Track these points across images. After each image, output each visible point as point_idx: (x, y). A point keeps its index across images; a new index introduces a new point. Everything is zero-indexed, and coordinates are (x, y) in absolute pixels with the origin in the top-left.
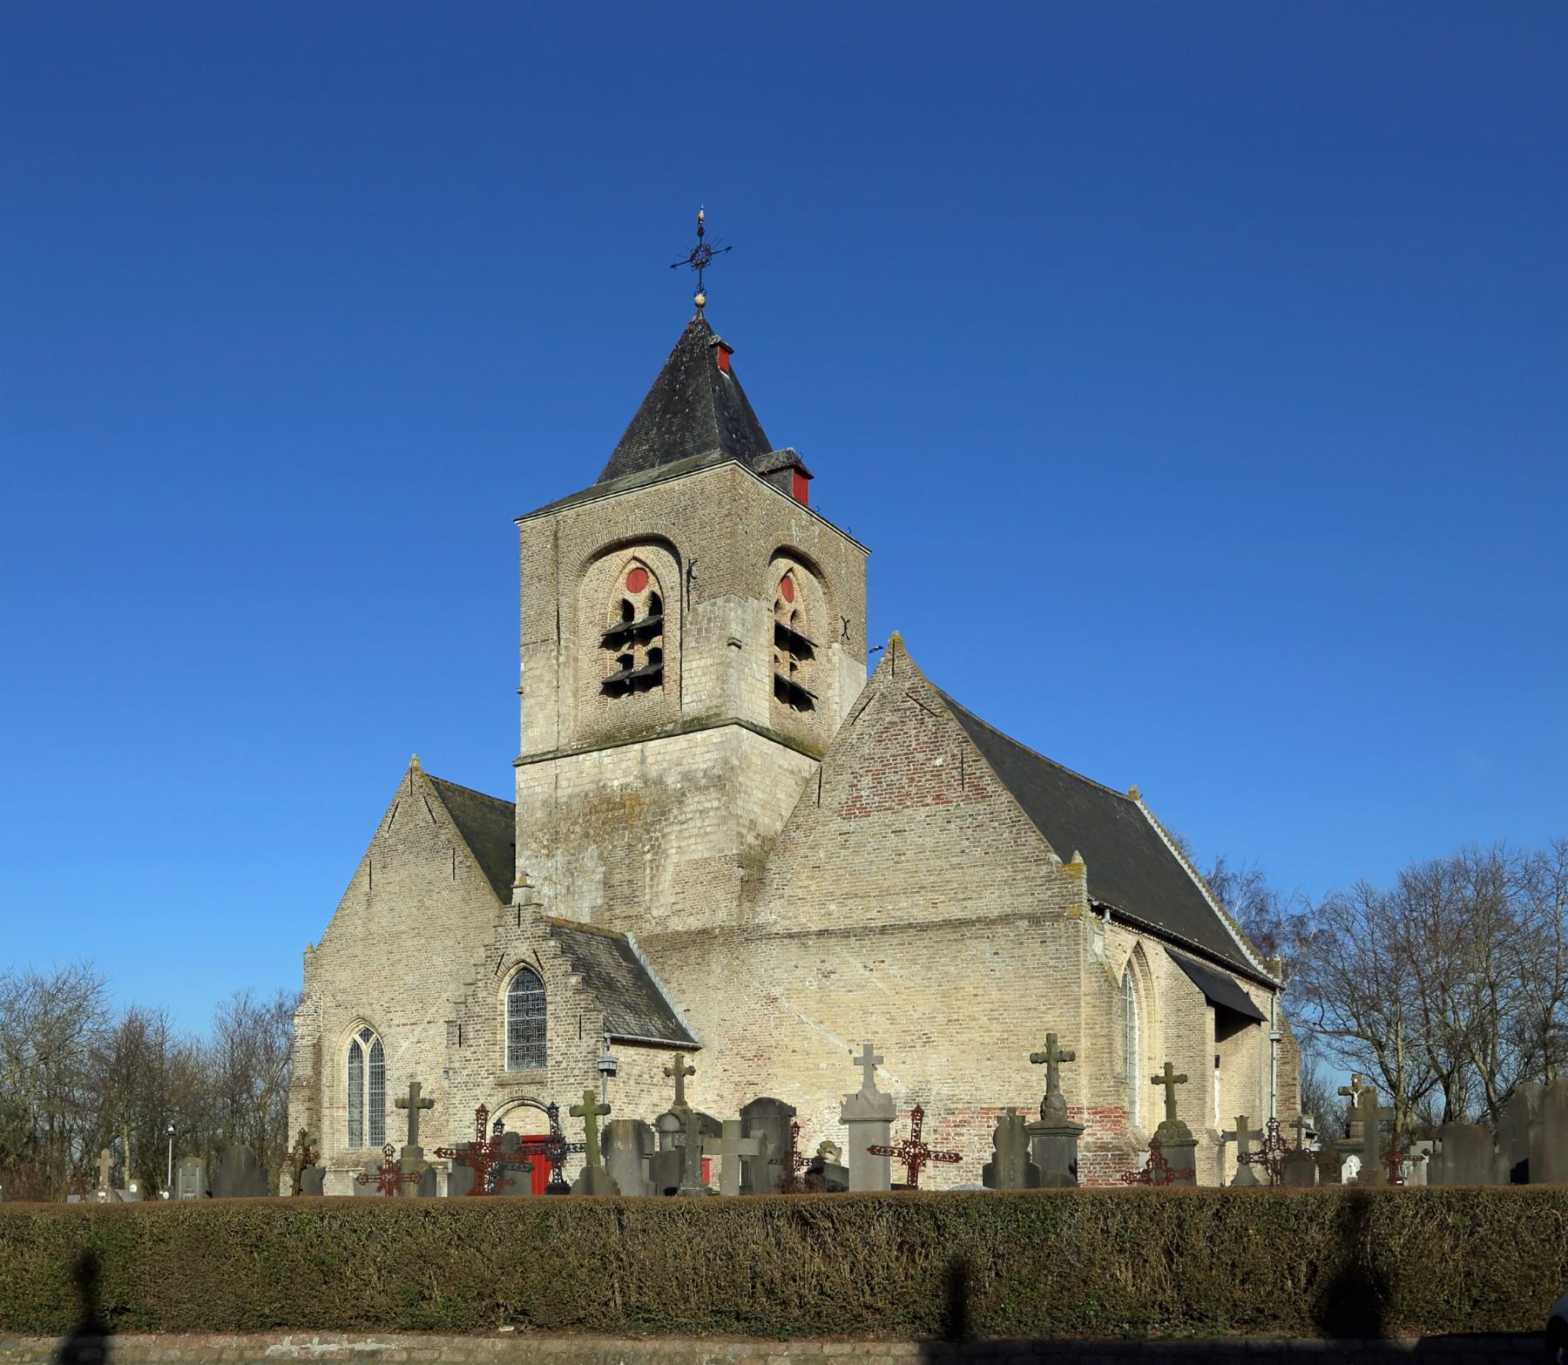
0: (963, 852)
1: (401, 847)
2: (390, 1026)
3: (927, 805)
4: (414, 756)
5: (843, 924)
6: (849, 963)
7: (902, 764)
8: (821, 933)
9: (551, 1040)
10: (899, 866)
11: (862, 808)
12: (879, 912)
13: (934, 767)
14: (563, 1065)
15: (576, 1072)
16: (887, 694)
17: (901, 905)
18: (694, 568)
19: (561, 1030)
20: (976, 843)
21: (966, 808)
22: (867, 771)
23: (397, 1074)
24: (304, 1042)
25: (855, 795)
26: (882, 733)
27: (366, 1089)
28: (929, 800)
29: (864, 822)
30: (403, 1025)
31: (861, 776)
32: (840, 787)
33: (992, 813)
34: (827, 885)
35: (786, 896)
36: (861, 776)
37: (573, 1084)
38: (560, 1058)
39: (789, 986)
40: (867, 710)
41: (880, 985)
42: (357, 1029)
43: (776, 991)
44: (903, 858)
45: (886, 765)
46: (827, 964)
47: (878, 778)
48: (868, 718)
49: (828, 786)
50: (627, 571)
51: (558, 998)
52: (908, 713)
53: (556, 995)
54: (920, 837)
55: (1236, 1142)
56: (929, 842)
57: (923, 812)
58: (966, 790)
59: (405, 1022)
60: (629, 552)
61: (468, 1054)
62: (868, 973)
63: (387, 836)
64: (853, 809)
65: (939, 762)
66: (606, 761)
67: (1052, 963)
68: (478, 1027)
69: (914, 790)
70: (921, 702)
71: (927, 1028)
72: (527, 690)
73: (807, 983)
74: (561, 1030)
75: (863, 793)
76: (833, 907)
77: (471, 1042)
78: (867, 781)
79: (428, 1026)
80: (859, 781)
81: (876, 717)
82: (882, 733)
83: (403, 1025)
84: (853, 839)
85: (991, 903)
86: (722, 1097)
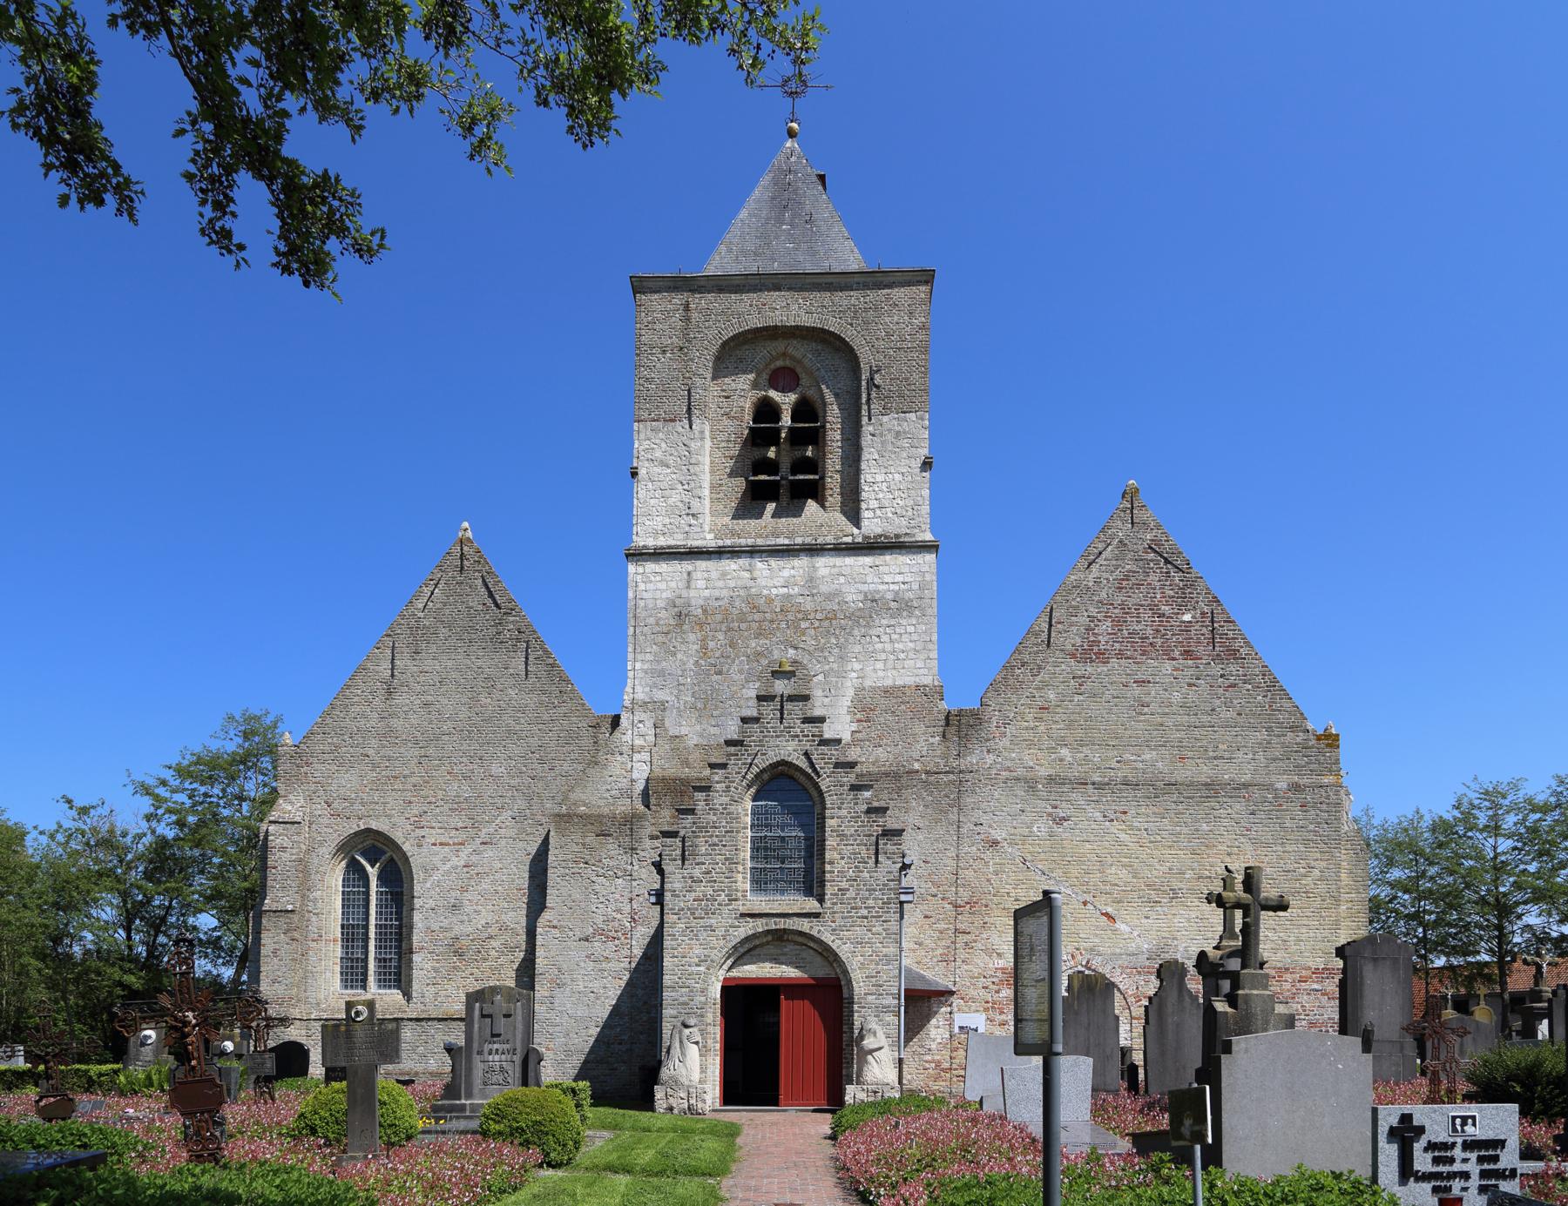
0: (1213, 710)
1: (443, 632)
2: (420, 846)
3: (1174, 659)
4: (466, 524)
5: (1075, 773)
6: (1087, 814)
7: (1146, 615)
8: (1051, 779)
9: (831, 863)
10: (1142, 718)
11: (1100, 653)
12: (1118, 762)
13: (1181, 622)
14: (851, 894)
15: (871, 902)
16: (1126, 542)
17: (1143, 757)
18: (877, 376)
19: (847, 851)
20: (1228, 704)
21: (1216, 669)
22: (1106, 617)
23: (431, 903)
24: (286, 856)
25: (1092, 639)
26: (1123, 580)
27: (372, 921)
28: (1176, 654)
29: (1103, 669)
30: (441, 844)
31: (1099, 621)
32: (1074, 629)
33: (1245, 675)
34: (1058, 729)
35: (1008, 734)
36: (1099, 621)
37: (866, 918)
38: (844, 885)
39: (1013, 831)
40: (1103, 556)
41: (1123, 836)
42: (360, 847)
43: (998, 834)
44: (1146, 709)
45: (1127, 613)
46: (1058, 810)
47: (1118, 623)
48: (1105, 563)
49: (1059, 626)
50: (772, 366)
51: (844, 812)
52: (1152, 565)
53: (839, 808)
54: (1166, 690)
55: (1091, 1060)
56: (1176, 697)
57: (1168, 667)
58: (1217, 649)
59: (444, 840)
60: (780, 346)
61: (697, 873)
62: (1107, 823)
63: (421, 615)
64: (1091, 653)
65: (1187, 617)
66: (823, 572)
67: (1312, 827)
68: (715, 840)
69: (1159, 641)
70: (1165, 555)
71: (1176, 884)
72: (642, 472)
73: (1035, 829)
74: (847, 851)
75: (1100, 638)
76: (1064, 752)
77: (700, 859)
78: (1106, 626)
79: (482, 848)
80: (1096, 626)
81: (1114, 562)
82: (1123, 580)
83: (441, 844)
84: (1088, 686)
85: (1242, 768)
86: (920, 944)
